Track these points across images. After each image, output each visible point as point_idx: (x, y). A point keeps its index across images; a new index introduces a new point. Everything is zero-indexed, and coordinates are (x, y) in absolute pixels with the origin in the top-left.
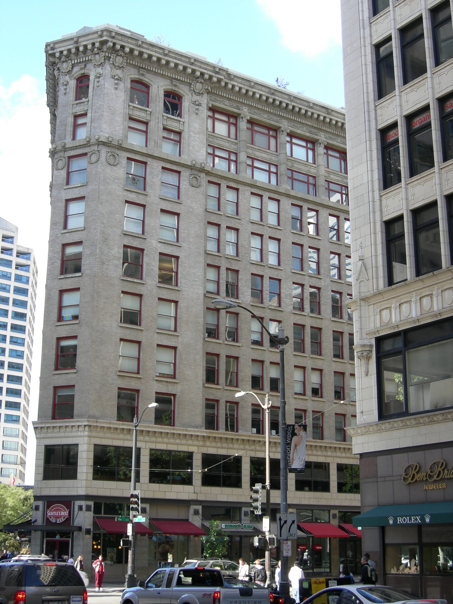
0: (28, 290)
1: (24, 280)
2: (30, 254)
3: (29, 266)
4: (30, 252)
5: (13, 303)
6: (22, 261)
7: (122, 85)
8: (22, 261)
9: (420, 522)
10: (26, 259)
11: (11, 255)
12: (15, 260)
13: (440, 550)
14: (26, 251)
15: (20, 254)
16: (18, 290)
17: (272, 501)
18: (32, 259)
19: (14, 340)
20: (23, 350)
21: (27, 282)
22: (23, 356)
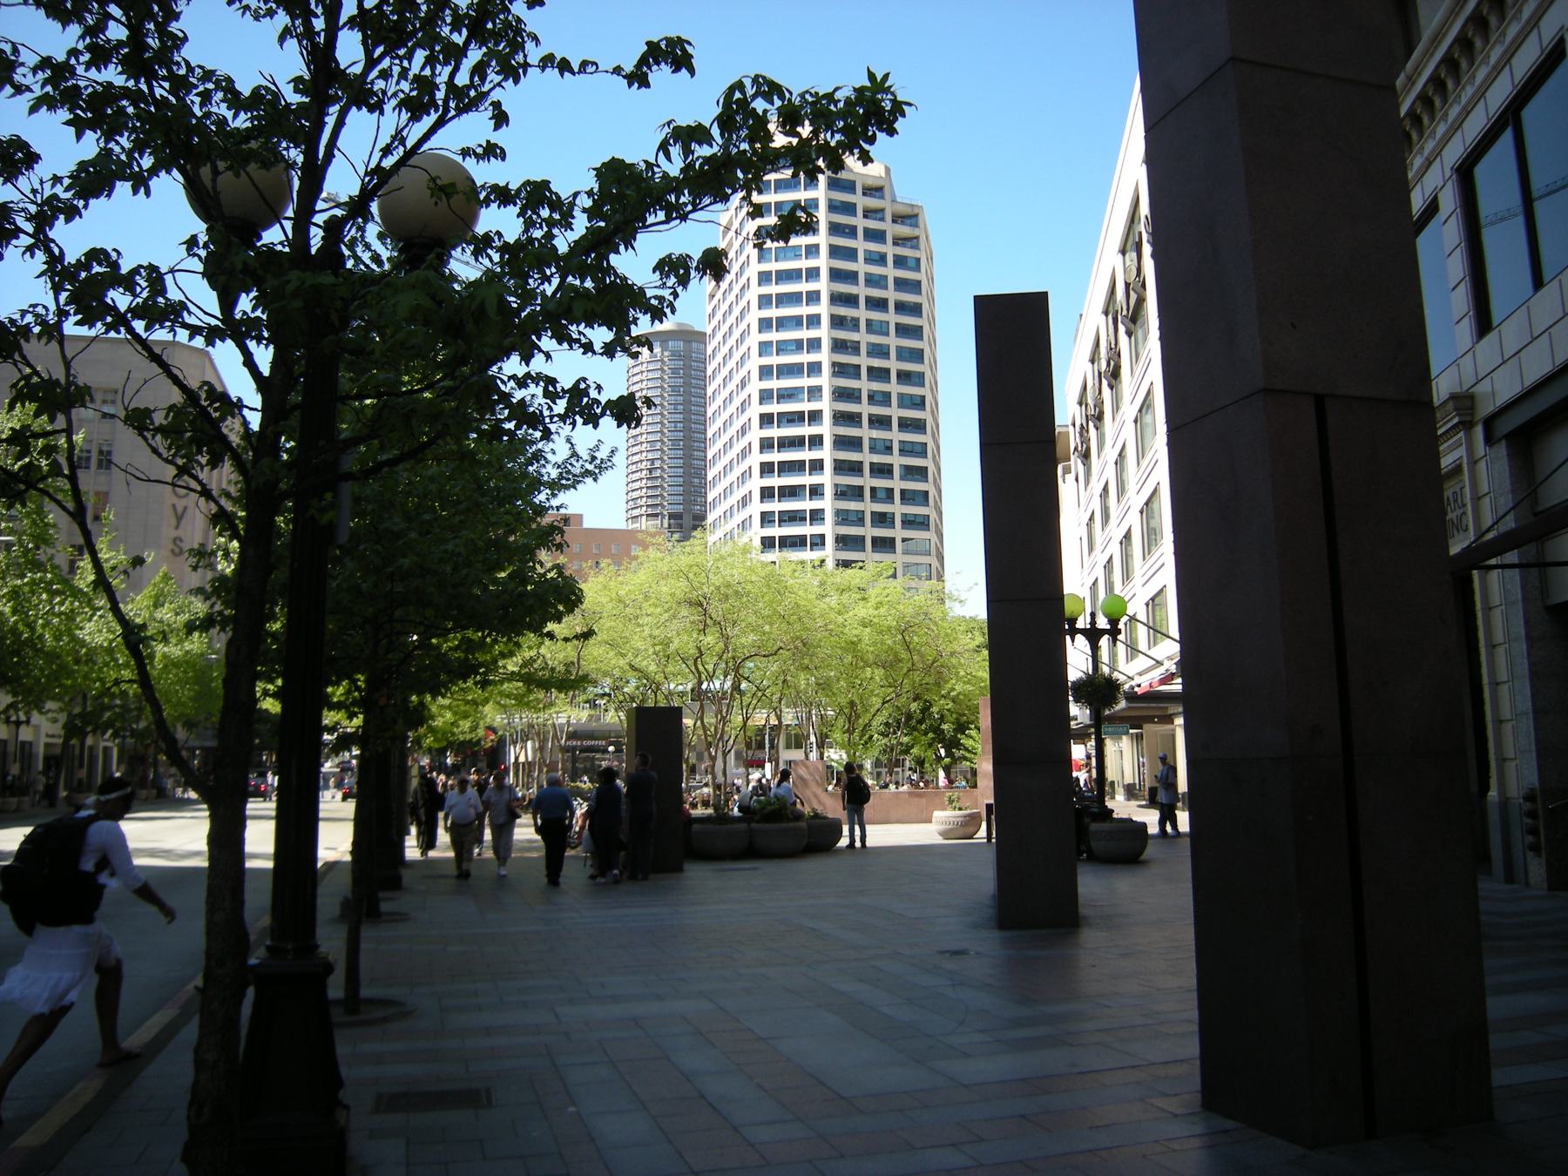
0: (922, 327)
1: (911, 263)
2: (916, 216)
3: (917, 238)
4: (916, 211)
5: (899, 425)
6: (904, 230)
7: (643, 166)
8: (904, 230)
9: (491, 373)
10: (912, 247)
11: (882, 219)
12: (892, 230)
13: (241, 1058)
14: (908, 211)
15: (898, 219)
16: (901, 284)
17: (165, 277)
18: (922, 226)
19: (908, 447)
20: (924, 441)
21: (917, 268)
22: (928, 525)
